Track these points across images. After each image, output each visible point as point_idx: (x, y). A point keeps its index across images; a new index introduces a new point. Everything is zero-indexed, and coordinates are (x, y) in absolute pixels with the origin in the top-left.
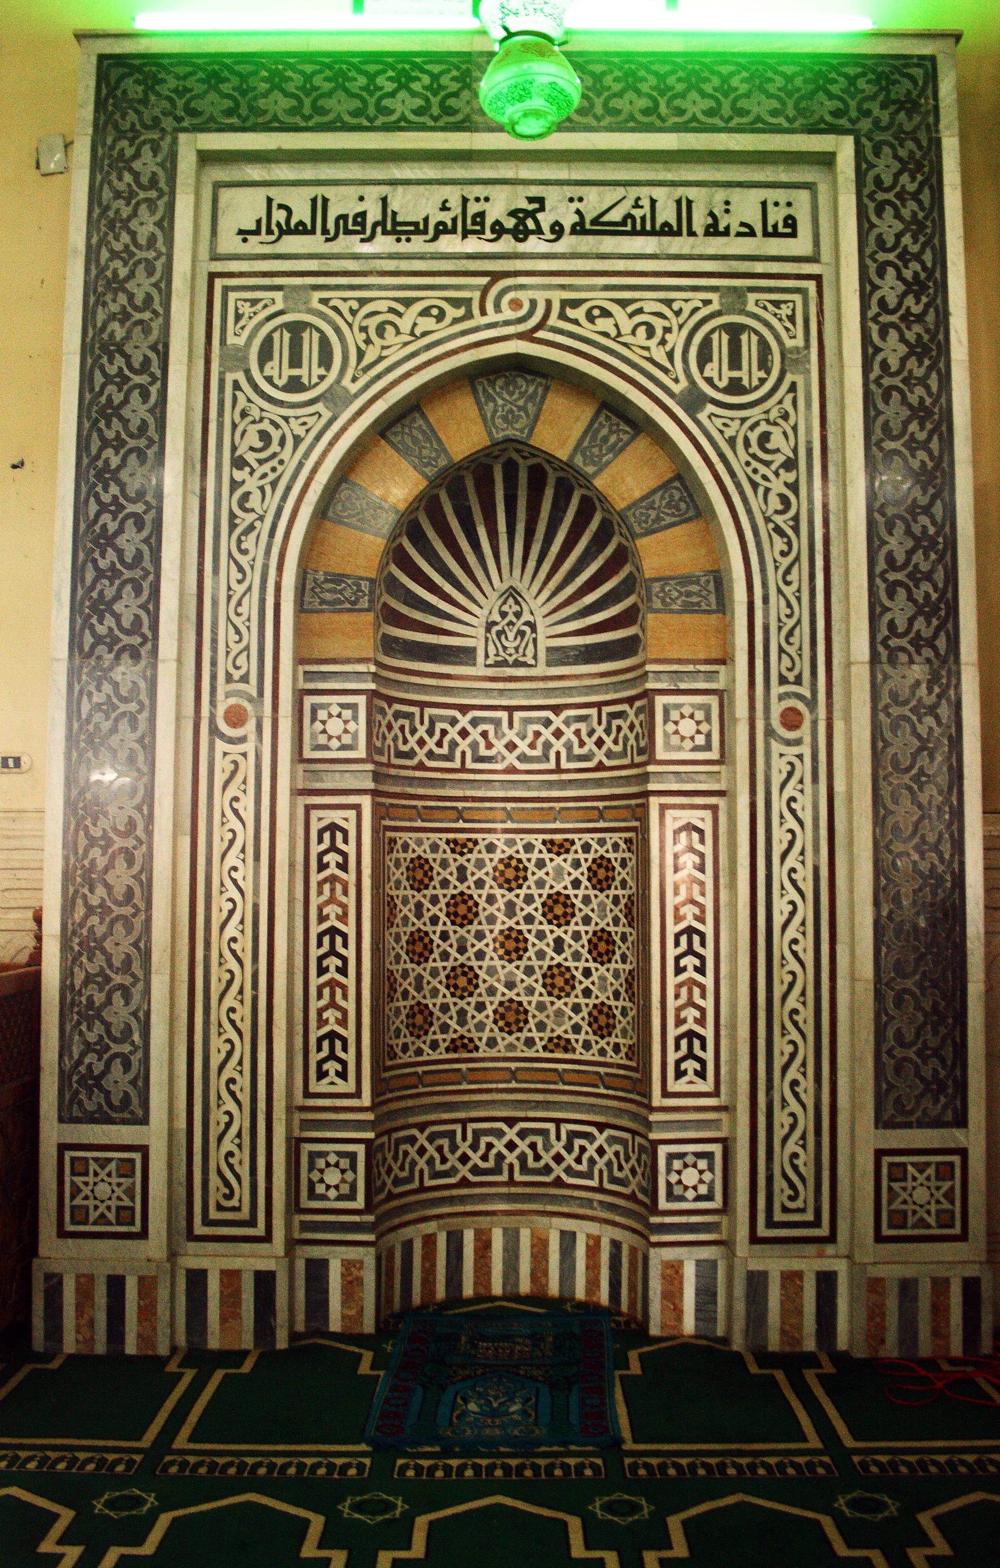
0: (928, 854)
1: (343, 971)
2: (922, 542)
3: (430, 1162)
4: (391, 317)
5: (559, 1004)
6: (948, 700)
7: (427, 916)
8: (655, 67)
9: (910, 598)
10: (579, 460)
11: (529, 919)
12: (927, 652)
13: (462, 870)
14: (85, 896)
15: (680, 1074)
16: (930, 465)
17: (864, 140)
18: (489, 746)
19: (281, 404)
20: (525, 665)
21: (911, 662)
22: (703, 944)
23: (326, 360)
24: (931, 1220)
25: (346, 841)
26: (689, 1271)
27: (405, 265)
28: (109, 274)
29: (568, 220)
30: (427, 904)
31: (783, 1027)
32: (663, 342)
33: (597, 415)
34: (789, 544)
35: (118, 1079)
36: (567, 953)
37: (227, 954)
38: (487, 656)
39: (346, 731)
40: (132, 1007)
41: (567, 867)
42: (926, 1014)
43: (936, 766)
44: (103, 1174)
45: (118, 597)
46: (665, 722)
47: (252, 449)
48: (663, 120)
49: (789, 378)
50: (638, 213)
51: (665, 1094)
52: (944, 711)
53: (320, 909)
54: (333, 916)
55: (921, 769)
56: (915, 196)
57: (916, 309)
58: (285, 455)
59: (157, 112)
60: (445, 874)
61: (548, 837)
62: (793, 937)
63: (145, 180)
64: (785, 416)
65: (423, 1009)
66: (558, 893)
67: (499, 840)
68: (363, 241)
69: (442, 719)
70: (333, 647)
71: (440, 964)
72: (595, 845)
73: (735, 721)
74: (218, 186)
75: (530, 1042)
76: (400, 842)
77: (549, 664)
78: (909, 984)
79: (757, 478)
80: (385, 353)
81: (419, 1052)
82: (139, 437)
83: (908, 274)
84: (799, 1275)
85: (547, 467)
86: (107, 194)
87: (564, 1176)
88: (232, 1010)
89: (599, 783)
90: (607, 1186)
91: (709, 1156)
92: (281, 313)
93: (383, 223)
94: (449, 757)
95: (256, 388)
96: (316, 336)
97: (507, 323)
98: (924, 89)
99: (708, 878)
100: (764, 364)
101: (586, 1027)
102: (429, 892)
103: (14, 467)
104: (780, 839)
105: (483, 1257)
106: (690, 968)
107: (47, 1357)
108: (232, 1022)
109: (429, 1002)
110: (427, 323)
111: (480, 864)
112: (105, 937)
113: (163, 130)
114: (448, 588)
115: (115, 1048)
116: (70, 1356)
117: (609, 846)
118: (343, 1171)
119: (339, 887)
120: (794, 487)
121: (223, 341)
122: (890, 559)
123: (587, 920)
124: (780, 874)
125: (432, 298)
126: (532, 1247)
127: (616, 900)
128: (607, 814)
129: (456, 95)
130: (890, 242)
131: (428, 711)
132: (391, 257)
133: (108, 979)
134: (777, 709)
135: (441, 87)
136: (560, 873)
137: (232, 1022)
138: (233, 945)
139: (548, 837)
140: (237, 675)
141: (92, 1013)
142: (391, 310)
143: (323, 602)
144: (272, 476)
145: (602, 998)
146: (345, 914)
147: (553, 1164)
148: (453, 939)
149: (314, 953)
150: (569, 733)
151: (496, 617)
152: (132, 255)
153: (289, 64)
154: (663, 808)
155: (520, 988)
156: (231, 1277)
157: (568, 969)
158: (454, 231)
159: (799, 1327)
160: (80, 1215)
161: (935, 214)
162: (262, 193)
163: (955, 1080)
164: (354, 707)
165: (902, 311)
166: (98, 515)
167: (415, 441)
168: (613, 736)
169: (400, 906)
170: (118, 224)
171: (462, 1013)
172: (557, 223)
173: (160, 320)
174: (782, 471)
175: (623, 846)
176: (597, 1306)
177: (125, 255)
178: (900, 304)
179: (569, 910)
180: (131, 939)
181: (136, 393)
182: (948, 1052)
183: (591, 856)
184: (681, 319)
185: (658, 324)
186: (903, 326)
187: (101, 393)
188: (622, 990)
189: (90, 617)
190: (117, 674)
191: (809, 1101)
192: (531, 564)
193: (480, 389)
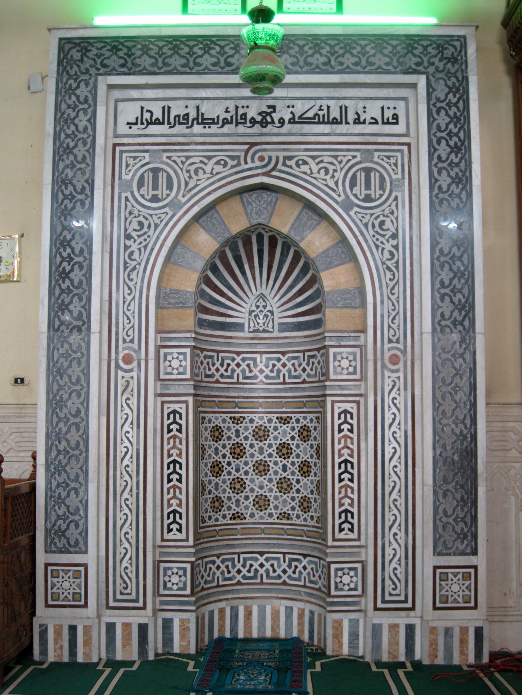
0: (63, 416)
1: (180, 481)
2: (457, 274)
3: (222, 573)
4: (201, 165)
5: (285, 496)
6: (470, 351)
7: (220, 454)
9: (452, 301)
11: (270, 455)
12: (460, 328)
13: (237, 431)
14: (57, 446)
15: (341, 530)
17: (431, 77)
18: (251, 371)
19: (148, 208)
20: (268, 331)
21: (452, 332)
22: (352, 467)
23: (170, 187)
24: (460, 599)
26: (346, 625)
27: (208, 140)
28: (65, 145)
29: (287, 117)
30: (220, 448)
31: (390, 508)
32: (333, 177)
33: (302, 211)
34: (394, 275)
35: (73, 533)
36: (289, 472)
37: (124, 473)
38: (249, 327)
39: (181, 366)
40: (80, 498)
41: (289, 430)
42: (458, 502)
43: (464, 383)
44: (66, 577)
45: (71, 302)
46: (335, 360)
47: (135, 230)
48: (333, 68)
49: (394, 194)
50: (321, 113)
51: (334, 540)
52: (468, 356)
53: (169, 451)
54: (175, 455)
55: (456, 384)
56: (456, 105)
57: (456, 160)
58: (151, 233)
59: (87, 66)
60: (229, 434)
61: (279, 415)
62: (395, 464)
63: (82, 99)
64: (392, 213)
65: (218, 499)
66: (284, 443)
68: (187, 127)
69: (227, 358)
70: (172, 324)
71: (227, 477)
74: (117, 101)
75: (271, 515)
76: (207, 419)
77: (280, 331)
78: (450, 487)
79: (378, 243)
80: (198, 183)
81: (217, 520)
83: (452, 143)
84: (397, 626)
85: (277, 236)
86: (64, 106)
89: (304, 389)
91: (355, 569)
92: (148, 163)
93: (197, 119)
94: (231, 377)
95: (136, 200)
96: (165, 175)
97: (257, 168)
98: (460, 51)
99: (355, 436)
100: (382, 187)
101: (297, 508)
102: (221, 443)
104: (389, 418)
105: (248, 619)
106: (346, 479)
107: (42, 663)
108: (127, 505)
109: (222, 495)
110: (218, 168)
112: (66, 465)
113: (90, 75)
114: (230, 294)
115: (71, 518)
116: (52, 663)
117: (308, 420)
118: (180, 577)
119: (177, 441)
120: (396, 247)
121: (120, 178)
124: (388, 434)
125: (221, 156)
126: (272, 614)
127: (312, 446)
130: (443, 127)
131: (221, 355)
132: (201, 135)
134: (387, 355)
135: (225, 53)
136: (285, 433)
137: (127, 505)
138: (127, 469)
139: (279, 415)
140: (128, 339)
141: (60, 501)
142: (201, 162)
143: (169, 303)
144: (144, 243)
145: (305, 494)
146: (181, 453)
147: (282, 574)
148: (233, 465)
149: (166, 472)
150: (289, 365)
151: (254, 308)
153: (151, 42)
154: (333, 402)
155: (266, 489)
156: (127, 626)
157: (289, 479)
158: (231, 123)
159: (397, 651)
161: (465, 114)
162: (139, 104)
163: (472, 533)
164: (184, 354)
165: (449, 161)
166: (61, 262)
167: (213, 225)
169: (207, 449)
170: (69, 121)
171: (238, 501)
173: (90, 168)
174: (390, 240)
175: (315, 420)
176: (302, 642)
178: (448, 158)
179: (290, 451)
180: (79, 466)
181: (79, 203)
182: (468, 520)
183: (300, 425)
184: (342, 165)
185: (331, 168)
186: (449, 169)
187: (62, 203)
188: (315, 490)
189: (57, 312)
190: (71, 340)
191: (402, 542)
192: (271, 282)
193: (245, 199)
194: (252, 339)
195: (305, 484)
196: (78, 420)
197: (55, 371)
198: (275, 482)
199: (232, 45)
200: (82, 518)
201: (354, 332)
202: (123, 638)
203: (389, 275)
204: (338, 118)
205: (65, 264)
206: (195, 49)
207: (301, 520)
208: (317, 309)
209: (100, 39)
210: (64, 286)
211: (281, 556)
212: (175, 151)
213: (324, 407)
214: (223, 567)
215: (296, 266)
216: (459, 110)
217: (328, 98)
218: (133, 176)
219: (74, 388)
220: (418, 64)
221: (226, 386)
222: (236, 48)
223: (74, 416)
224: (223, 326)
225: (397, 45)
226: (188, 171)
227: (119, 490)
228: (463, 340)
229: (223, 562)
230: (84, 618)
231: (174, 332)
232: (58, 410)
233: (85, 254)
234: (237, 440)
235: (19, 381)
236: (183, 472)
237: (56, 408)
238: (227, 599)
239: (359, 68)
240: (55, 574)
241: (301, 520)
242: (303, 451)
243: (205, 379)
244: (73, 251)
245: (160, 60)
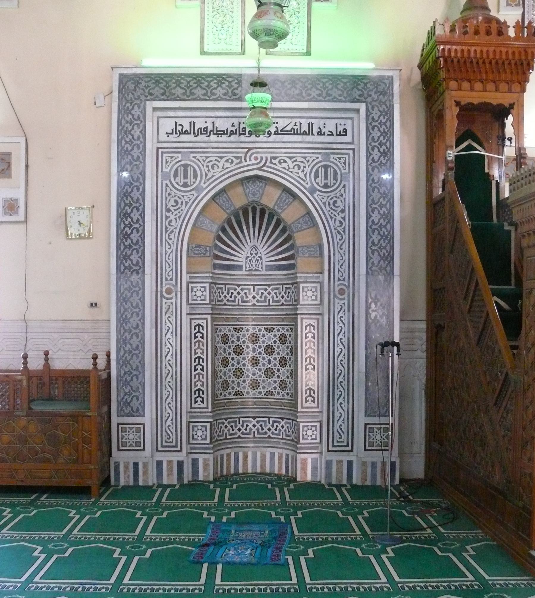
1: (202, 370)
2: (383, 237)
3: (229, 430)
8: (302, 80)
10: (276, 208)
11: (260, 353)
12: (384, 272)
13: (238, 337)
15: (306, 401)
16: (386, 212)
18: (247, 297)
19: (181, 191)
20: (258, 270)
21: (379, 274)
25: (203, 329)
28: (125, 149)
30: (227, 348)
32: (303, 171)
34: (342, 237)
35: (135, 404)
36: (272, 364)
40: (139, 381)
41: (272, 337)
44: (131, 432)
45: (131, 254)
48: (304, 98)
50: (295, 128)
51: (302, 407)
53: (195, 350)
58: (183, 207)
59: (139, 94)
60: (233, 339)
62: (341, 359)
63: (136, 117)
64: (342, 195)
67: (250, 328)
69: (231, 289)
71: (231, 368)
72: (281, 330)
73: (324, 292)
74: (159, 118)
75: (260, 393)
79: (332, 216)
81: (225, 396)
83: (381, 150)
86: (123, 122)
90: (284, 437)
91: (316, 426)
92: (321, 162)
93: (213, 131)
94: (234, 301)
95: (173, 186)
96: (192, 169)
97: (253, 164)
99: (316, 341)
100: (335, 178)
102: (228, 345)
109: (228, 380)
110: (228, 165)
111: (244, 336)
114: (234, 246)
115: (134, 394)
119: (201, 344)
120: (344, 218)
122: (373, 242)
123: (278, 354)
124: (337, 340)
127: (288, 347)
128: (285, 320)
129: (237, 89)
130: (376, 139)
131: (227, 286)
132: (216, 142)
133: (131, 373)
134: (337, 289)
135: (232, 86)
136: (270, 339)
141: (127, 383)
142: (216, 160)
143: (195, 254)
144: (179, 215)
145: (283, 378)
146: (203, 352)
148: (235, 360)
150: (273, 293)
152: (132, 142)
154: (302, 319)
155: (257, 375)
156: (170, 463)
158: (236, 133)
159: (342, 477)
160: (124, 444)
164: (205, 287)
166: (124, 228)
171: (238, 383)
172: (269, 131)
178: (379, 160)
183: (280, 333)
185: (302, 165)
194: (248, 275)
195: (283, 372)
196: (137, 331)
197: (122, 300)
199: (236, 81)
201: (316, 273)
202: (168, 470)
203: (339, 237)
204: (307, 131)
205: (127, 229)
206: (212, 84)
207: (281, 396)
209: (147, 75)
211: (267, 419)
212: (198, 152)
213: (296, 322)
214: (229, 427)
215: (286, 243)
216: (387, 128)
217: (300, 118)
219: (135, 310)
220: (360, 96)
221: (231, 307)
222: (239, 83)
223: (135, 329)
224: (229, 267)
225: (347, 83)
226: (207, 166)
227: (164, 375)
229: (229, 423)
230: (142, 457)
231: (199, 273)
233: (141, 222)
234: (238, 343)
236: (205, 364)
238: (232, 448)
240: (124, 430)
241: (281, 396)
242: (282, 351)
243: (217, 303)
244: (132, 220)
245: (188, 91)
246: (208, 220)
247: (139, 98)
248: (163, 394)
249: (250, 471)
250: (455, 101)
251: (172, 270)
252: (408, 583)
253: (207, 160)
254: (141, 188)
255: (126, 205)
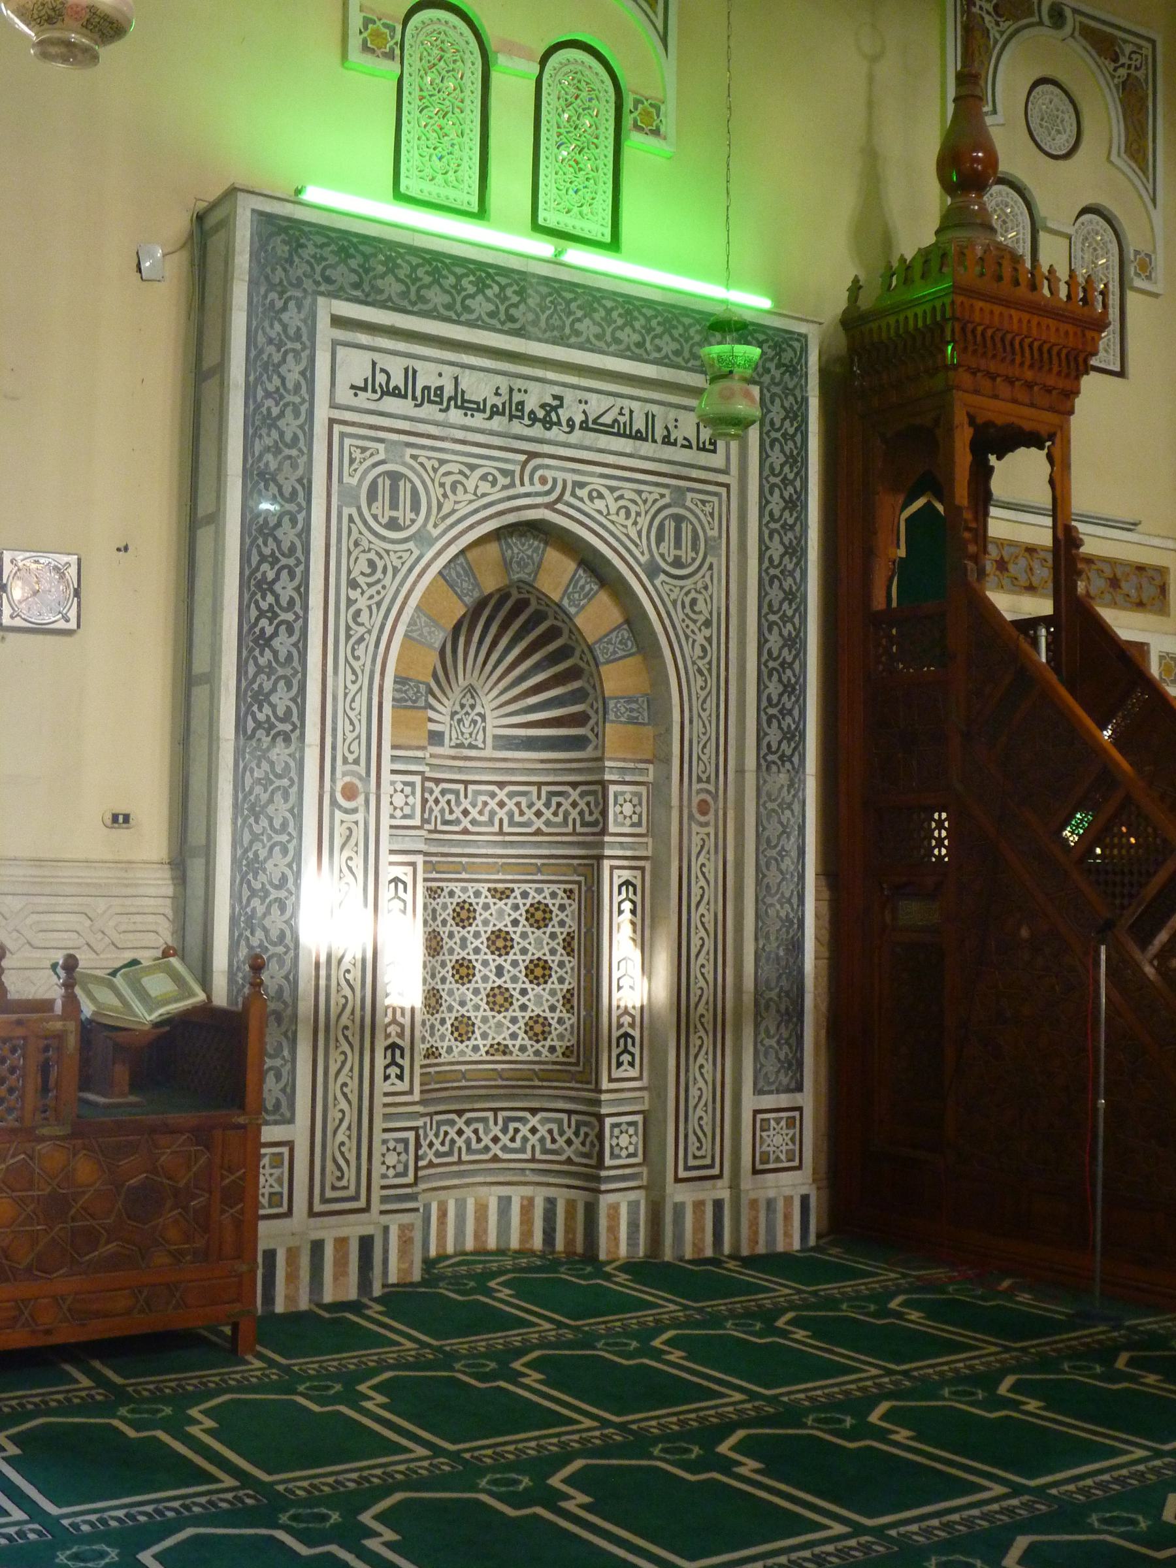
5: (499, 1017)
10: (565, 602)
11: (477, 951)
12: (788, 765)
14: (247, 939)
19: (383, 538)
24: (783, 1157)
26: (624, 1210)
27: (471, 437)
32: (635, 523)
36: (507, 977)
41: (508, 909)
43: (791, 844)
45: (274, 690)
46: (615, 803)
47: (362, 573)
49: (709, 559)
50: (622, 419)
51: (611, 1080)
57: (790, 521)
58: (387, 581)
61: (492, 885)
64: (706, 588)
72: (532, 893)
75: (476, 1049)
76: (446, 891)
77: (494, 748)
79: (688, 632)
82: (289, 556)
86: (261, 340)
87: (500, 1153)
88: (346, 1028)
93: (455, 398)
95: (365, 523)
97: (537, 494)
100: (695, 548)
103: (119, 550)
110: (485, 487)
113: (305, 290)
121: (340, 480)
123: (524, 951)
125: (489, 466)
129: (516, 306)
134: (695, 800)
139: (492, 885)
140: (351, 758)
142: (461, 472)
144: (377, 598)
154: (612, 868)
155: (469, 1005)
156: (341, 1242)
158: (503, 414)
159: (702, 1240)
162: (368, 356)
166: (257, 619)
168: (553, 809)
177: (276, 396)
190: (273, 755)
194: (454, 758)
198: (483, 995)
199: (515, 287)
200: (286, 1061)
201: (642, 761)
205: (264, 622)
208: (579, 720)
210: (262, 661)
212: (423, 447)
218: (361, 481)
219: (277, 838)
226: (442, 485)
228: (791, 785)
232: (250, 876)
233: (297, 608)
235: (120, 820)
237: (247, 873)
239: (679, 360)
246: (423, 619)
247: (298, 284)
248: (331, 1062)
249: (450, 1249)
250: (968, 414)
251: (358, 737)
252: (80, 1516)
253: (442, 470)
254: (300, 517)
255: (263, 559)
